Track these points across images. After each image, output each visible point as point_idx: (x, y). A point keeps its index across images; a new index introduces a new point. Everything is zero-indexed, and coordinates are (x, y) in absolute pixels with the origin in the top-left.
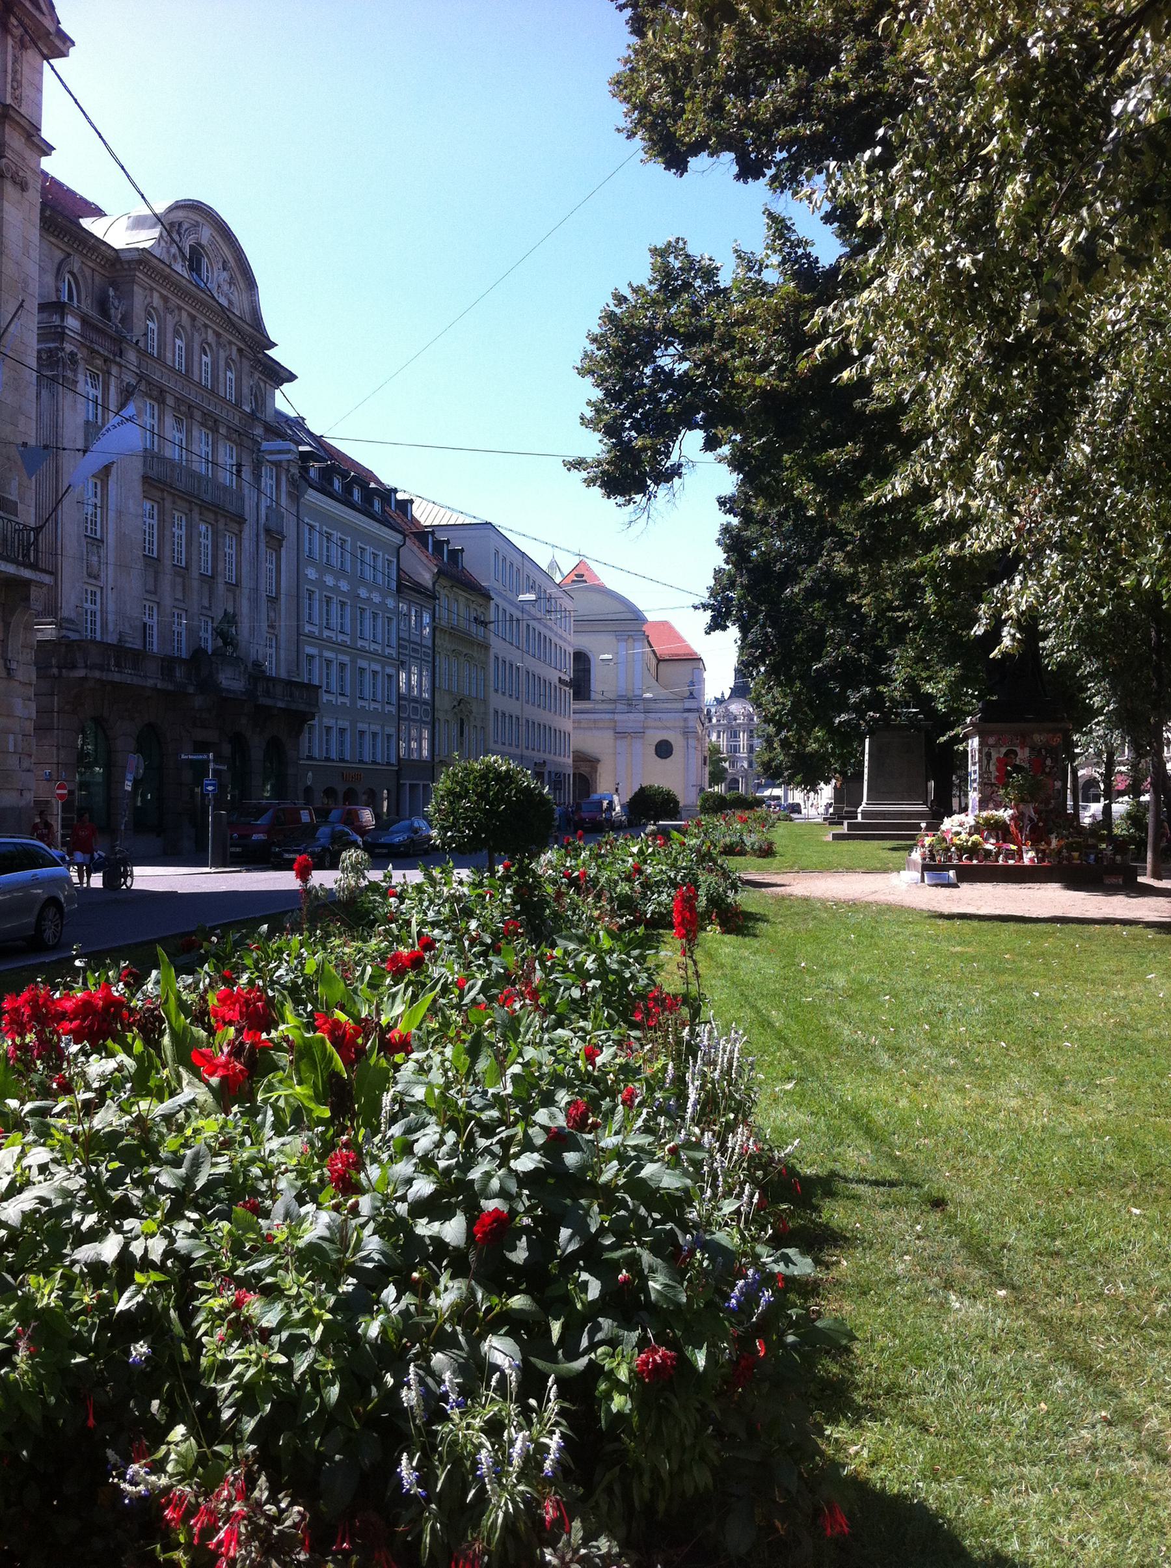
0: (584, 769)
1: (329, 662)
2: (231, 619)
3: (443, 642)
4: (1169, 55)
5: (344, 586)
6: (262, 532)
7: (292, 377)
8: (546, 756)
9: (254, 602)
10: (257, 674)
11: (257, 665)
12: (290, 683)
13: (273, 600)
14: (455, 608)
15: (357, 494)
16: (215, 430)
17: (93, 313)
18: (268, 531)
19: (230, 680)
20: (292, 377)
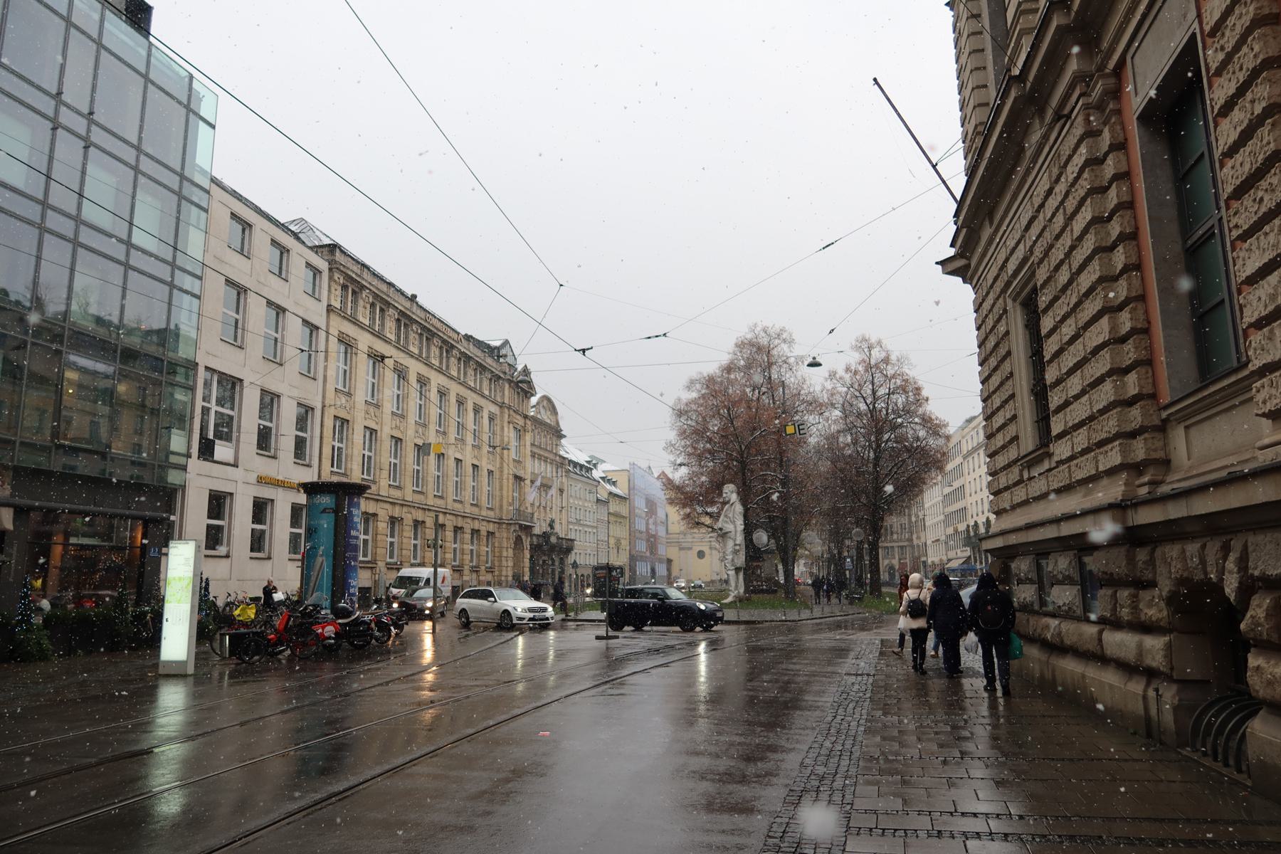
2: (553, 521)
3: (612, 519)
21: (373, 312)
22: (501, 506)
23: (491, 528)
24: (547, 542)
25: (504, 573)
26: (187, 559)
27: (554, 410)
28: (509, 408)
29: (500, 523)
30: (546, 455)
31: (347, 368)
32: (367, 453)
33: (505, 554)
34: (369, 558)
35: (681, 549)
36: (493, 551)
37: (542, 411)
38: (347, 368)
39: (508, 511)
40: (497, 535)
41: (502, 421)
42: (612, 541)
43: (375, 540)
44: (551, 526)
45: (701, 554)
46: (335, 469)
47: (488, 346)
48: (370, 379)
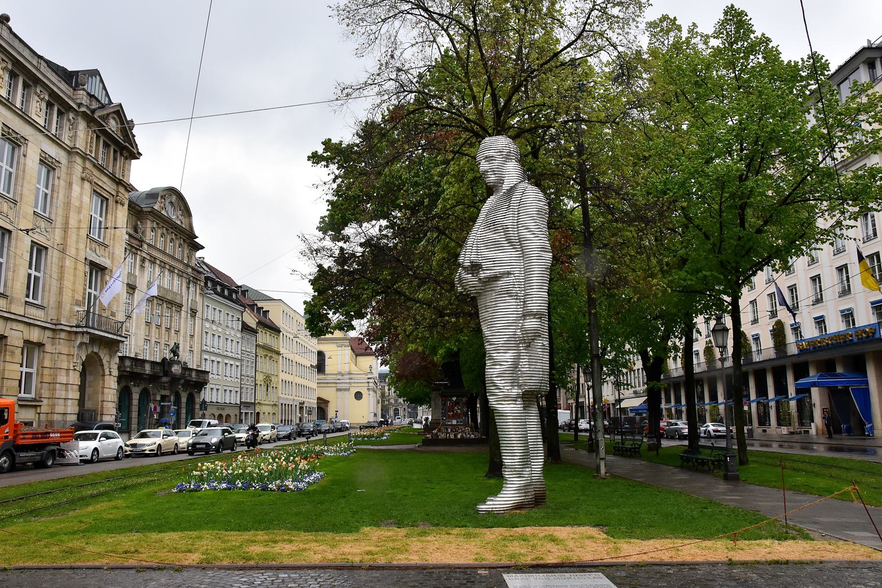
0: (323, 406)
1: (213, 361)
2: (177, 346)
3: (261, 352)
4: (881, 89)
5: (220, 330)
6: (59, 222)
7: (203, 248)
8: (304, 399)
9: (185, 337)
10: (185, 368)
11: (185, 363)
12: (197, 371)
13: (192, 336)
14: (264, 337)
15: (226, 293)
16: (154, 263)
17: (132, 232)
18: (191, 309)
19: (176, 369)
20: (203, 248)
21: (49, 114)
22: (60, 305)
23: (35, 335)
24: (167, 373)
25: (59, 409)
26: (89, 399)
27: (187, 211)
28: (84, 157)
29: (55, 330)
30: (166, 259)
31: (49, 192)
32: (33, 273)
33: (62, 379)
34: (33, 395)
35: (338, 390)
36: (40, 374)
37: (169, 207)
38: (49, 192)
39: (72, 313)
40: (48, 348)
41: (70, 174)
42: (260, 378)
43: (40, 374)
44: (175, 351)
45: (359, 396)
46: (30, 300)
47: (64, 70)
48: (42, 188)
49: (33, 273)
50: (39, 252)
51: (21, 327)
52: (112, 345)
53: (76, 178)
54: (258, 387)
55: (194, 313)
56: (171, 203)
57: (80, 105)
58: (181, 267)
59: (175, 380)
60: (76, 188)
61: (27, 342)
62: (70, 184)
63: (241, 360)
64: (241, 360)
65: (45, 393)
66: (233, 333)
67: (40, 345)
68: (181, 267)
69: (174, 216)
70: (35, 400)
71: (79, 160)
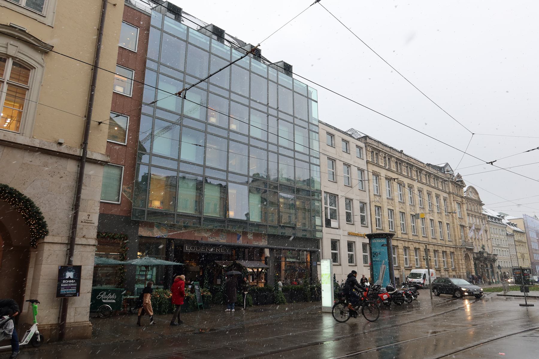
2: (483, 246)
3: (517, 243)
22: (456, 240)
23: (452, 250)
27: (477, 193)
31: (378, 185)
32: (390, 220)
33: (461, 262)
37: (470, 193)
38: (378, 185)
40: (455, 253)
41: (450, 201)
42: (519, 255)
44: (483, 248)
47: (439, 167)
48: (388, 189)
49: (377, 217)
50: (378, 209)
51: (441, 247)
52: (471, 250)
53: (452, 201)
54: (519, 260)
55: (486, 231)
56: (471, 192)
57: (449, 178)
58: (478, 215)
59: (486, 259)
60: (453, 204)
61: (404, 247)
62: (451, 203)
63: (508, 248)
64: (508, 248)
65: (457, 267)
66: (503, 237)
67: (453, 253)
68: (478, 215)
69: (472, 196)
70: (409, 267)
71: (452, 195)
